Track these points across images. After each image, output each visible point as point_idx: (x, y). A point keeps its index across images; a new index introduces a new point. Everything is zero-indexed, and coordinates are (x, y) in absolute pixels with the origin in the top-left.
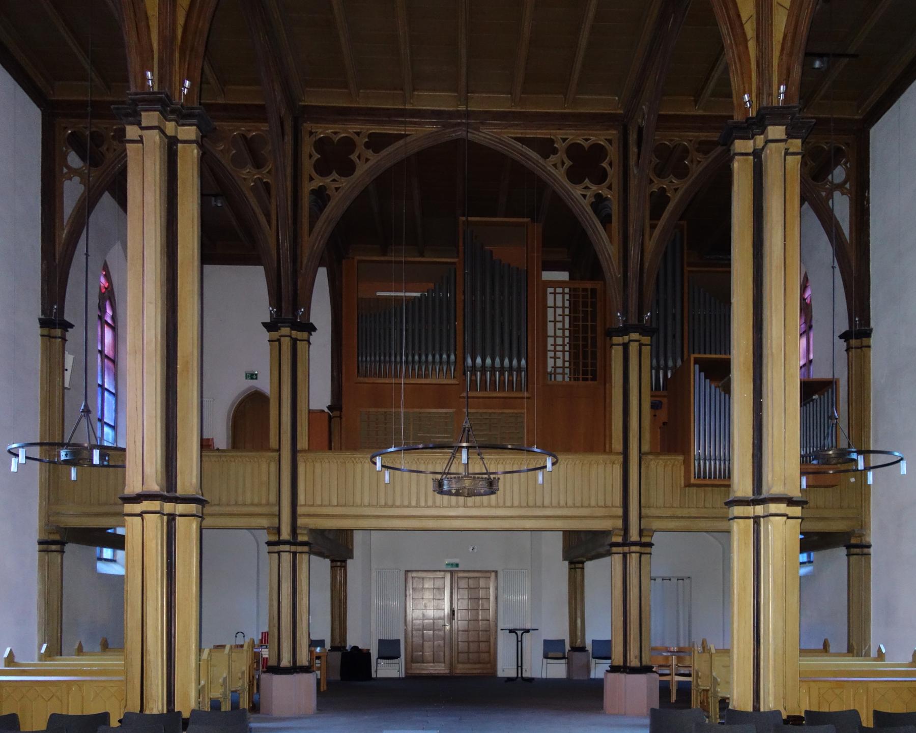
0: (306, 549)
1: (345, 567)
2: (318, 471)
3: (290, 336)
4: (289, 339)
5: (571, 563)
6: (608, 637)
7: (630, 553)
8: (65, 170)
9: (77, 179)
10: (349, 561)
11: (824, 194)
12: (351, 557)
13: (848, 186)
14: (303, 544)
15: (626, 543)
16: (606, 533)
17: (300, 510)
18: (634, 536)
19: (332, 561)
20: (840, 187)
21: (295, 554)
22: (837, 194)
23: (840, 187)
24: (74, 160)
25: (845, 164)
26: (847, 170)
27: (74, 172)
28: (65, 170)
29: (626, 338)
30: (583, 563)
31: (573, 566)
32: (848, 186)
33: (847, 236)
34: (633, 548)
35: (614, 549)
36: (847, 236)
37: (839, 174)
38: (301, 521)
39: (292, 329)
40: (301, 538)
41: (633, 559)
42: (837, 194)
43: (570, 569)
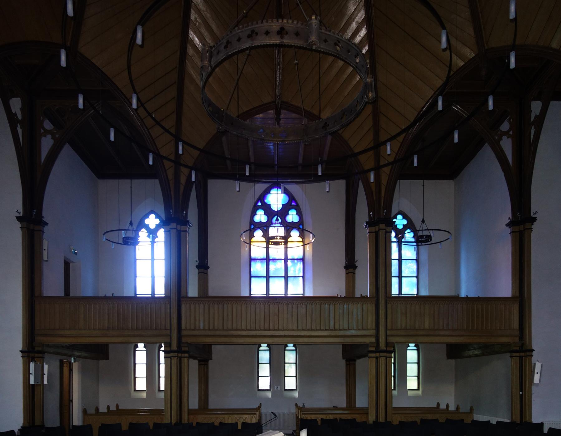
0: (186, 355)
1: (207, 365)
2: (192, 306)
3: (176, 229)
4: (175, 230)
5: (347, 361)
6: (367, 406)
7: (380, 357)
8: (42, 131)
9: (49, 137)
10: (210, 362)
11: (497, 137)
12: (463, 420)
13: (511, 133)
14: (185, 352)
15: (378, 351)
16: (366, 345)
17: (184, 333)
18: (382, 346)
19: (199, 361)
20: (506, 133)
21: (180, 358)
22: (505, 138)
23: (506, 133)
24: (48, 125)
25: (509, 119)
26: (510, 123)
27: (47, 132)
28: (42, 131)
29: (377, 228)
30: (355, 361)
31: (348, 363)
32: (511, 133)
33: (511, 162)
34: (382, 354)
35: (371, 355)
36: (511, 162)
37: (505, 126)
38: (184, 340)
39: (178, 224)
40: (183, 349)
41: (382, 361)
42: (505, 138)
43: (347, 365)
